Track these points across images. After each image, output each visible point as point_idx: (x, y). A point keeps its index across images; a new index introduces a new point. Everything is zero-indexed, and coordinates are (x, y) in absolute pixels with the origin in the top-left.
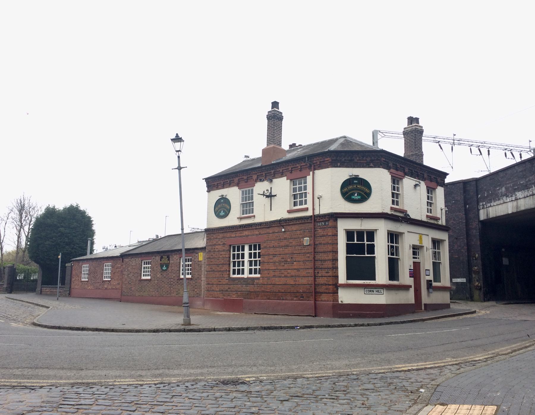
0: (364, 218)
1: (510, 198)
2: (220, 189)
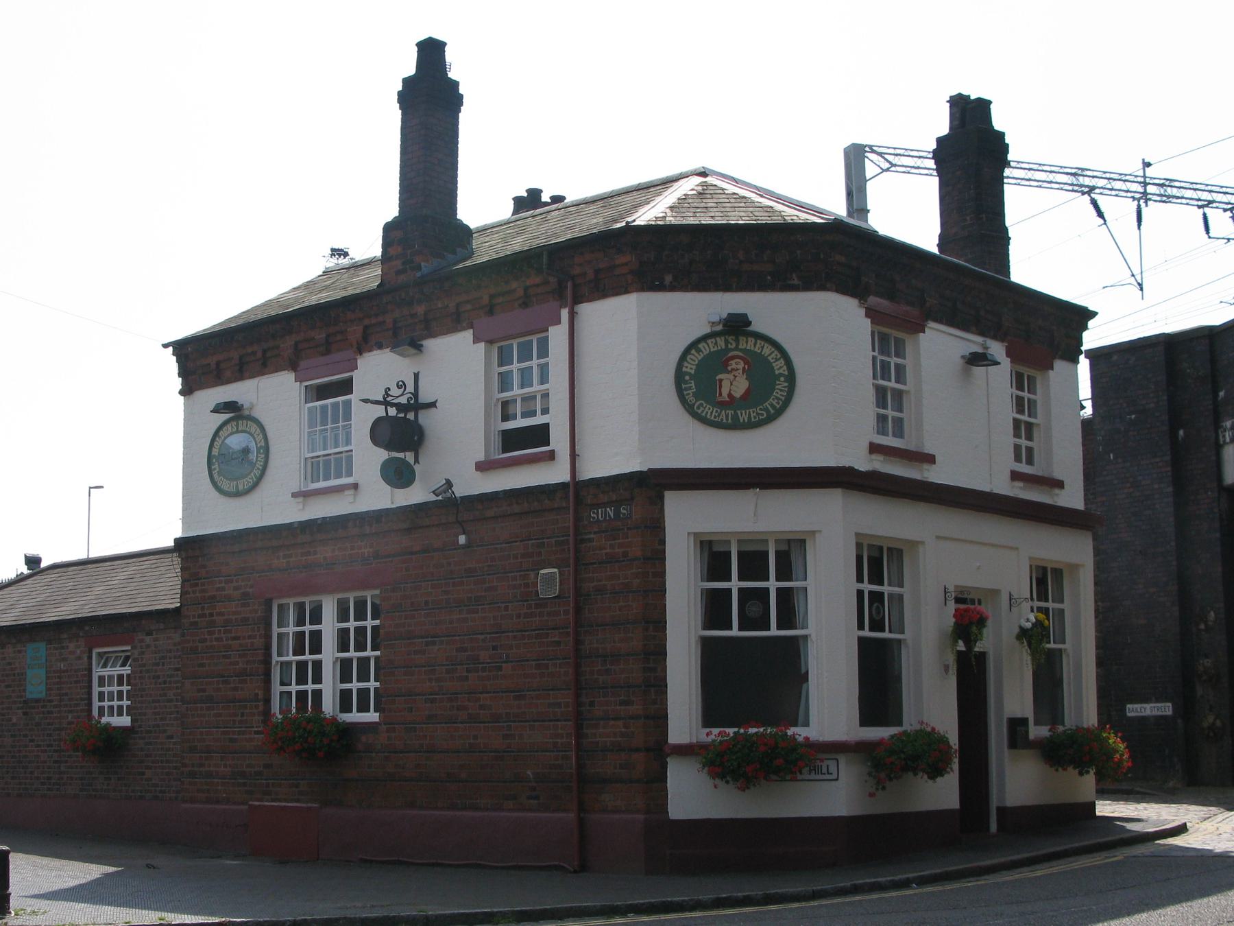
0: (765, 486)
2: (228, 382)
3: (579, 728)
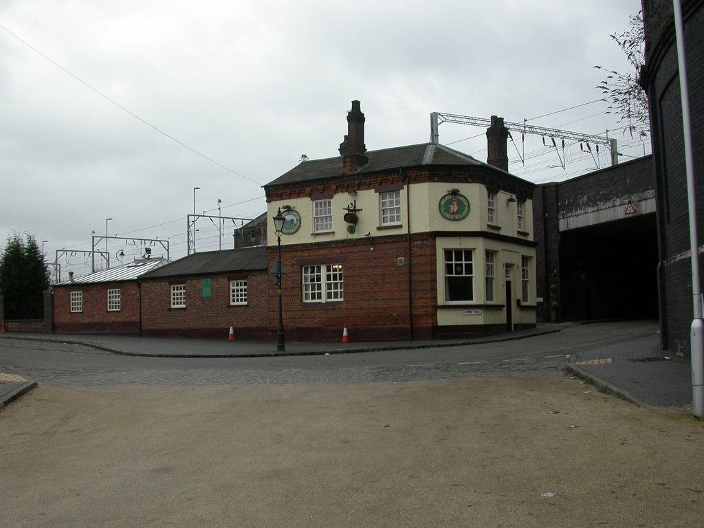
3: (411, 301)
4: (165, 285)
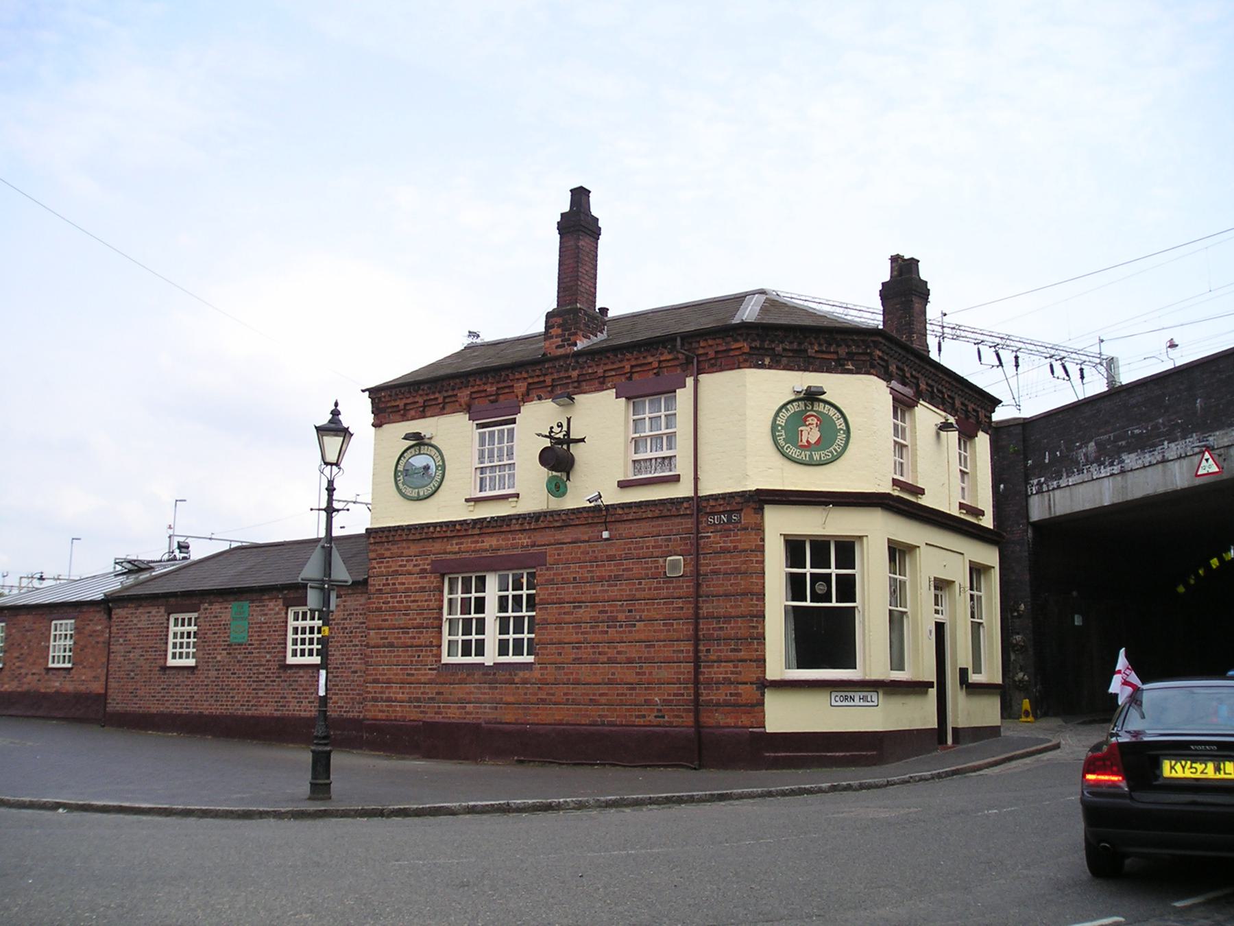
1: (1109, 469)
4: (157, 613)
